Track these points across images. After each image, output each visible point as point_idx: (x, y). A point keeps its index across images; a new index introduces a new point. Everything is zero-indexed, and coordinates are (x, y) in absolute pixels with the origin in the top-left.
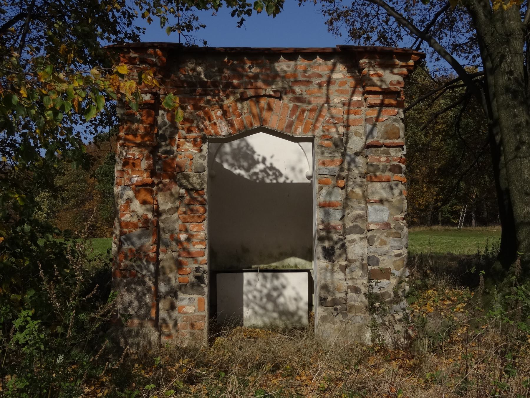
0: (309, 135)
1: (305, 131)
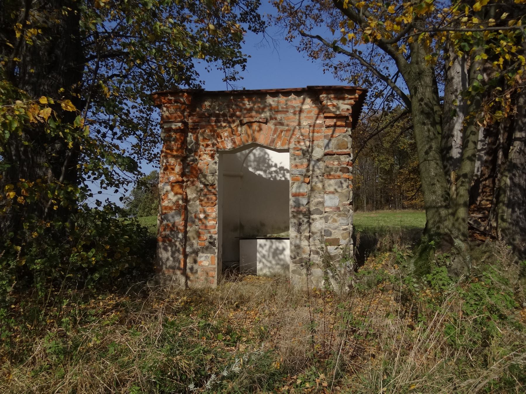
0: (286, 147)
1: (282, 145)
